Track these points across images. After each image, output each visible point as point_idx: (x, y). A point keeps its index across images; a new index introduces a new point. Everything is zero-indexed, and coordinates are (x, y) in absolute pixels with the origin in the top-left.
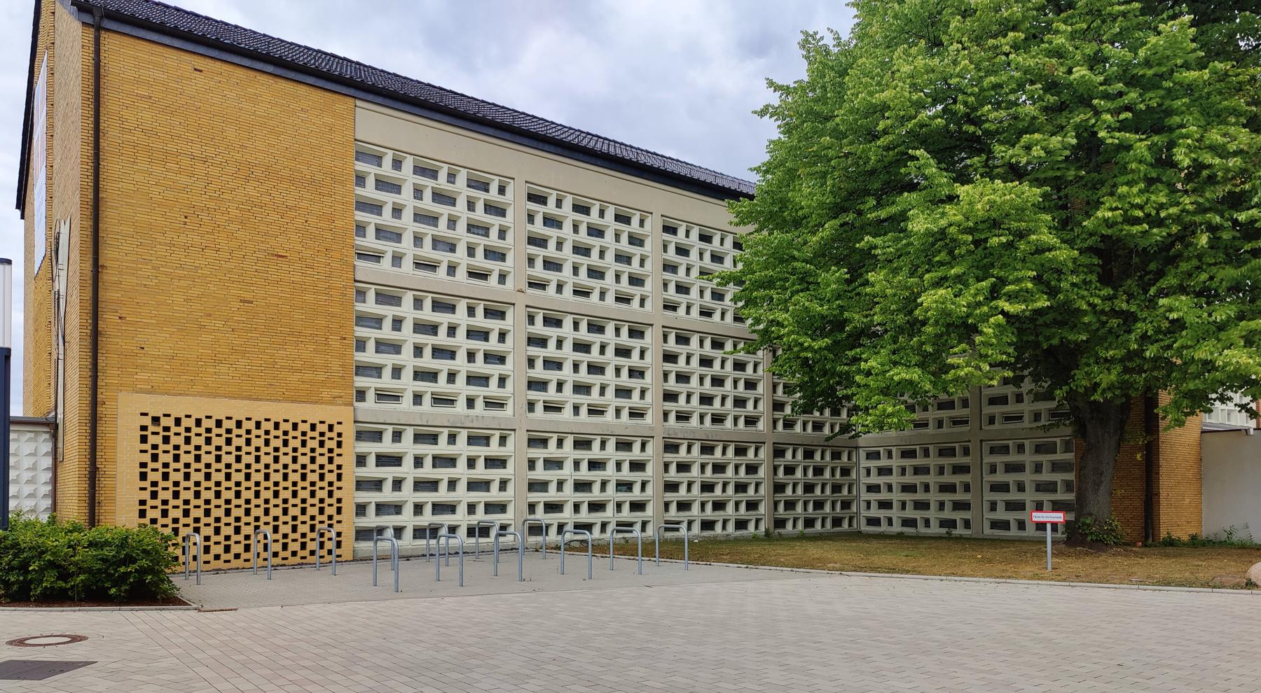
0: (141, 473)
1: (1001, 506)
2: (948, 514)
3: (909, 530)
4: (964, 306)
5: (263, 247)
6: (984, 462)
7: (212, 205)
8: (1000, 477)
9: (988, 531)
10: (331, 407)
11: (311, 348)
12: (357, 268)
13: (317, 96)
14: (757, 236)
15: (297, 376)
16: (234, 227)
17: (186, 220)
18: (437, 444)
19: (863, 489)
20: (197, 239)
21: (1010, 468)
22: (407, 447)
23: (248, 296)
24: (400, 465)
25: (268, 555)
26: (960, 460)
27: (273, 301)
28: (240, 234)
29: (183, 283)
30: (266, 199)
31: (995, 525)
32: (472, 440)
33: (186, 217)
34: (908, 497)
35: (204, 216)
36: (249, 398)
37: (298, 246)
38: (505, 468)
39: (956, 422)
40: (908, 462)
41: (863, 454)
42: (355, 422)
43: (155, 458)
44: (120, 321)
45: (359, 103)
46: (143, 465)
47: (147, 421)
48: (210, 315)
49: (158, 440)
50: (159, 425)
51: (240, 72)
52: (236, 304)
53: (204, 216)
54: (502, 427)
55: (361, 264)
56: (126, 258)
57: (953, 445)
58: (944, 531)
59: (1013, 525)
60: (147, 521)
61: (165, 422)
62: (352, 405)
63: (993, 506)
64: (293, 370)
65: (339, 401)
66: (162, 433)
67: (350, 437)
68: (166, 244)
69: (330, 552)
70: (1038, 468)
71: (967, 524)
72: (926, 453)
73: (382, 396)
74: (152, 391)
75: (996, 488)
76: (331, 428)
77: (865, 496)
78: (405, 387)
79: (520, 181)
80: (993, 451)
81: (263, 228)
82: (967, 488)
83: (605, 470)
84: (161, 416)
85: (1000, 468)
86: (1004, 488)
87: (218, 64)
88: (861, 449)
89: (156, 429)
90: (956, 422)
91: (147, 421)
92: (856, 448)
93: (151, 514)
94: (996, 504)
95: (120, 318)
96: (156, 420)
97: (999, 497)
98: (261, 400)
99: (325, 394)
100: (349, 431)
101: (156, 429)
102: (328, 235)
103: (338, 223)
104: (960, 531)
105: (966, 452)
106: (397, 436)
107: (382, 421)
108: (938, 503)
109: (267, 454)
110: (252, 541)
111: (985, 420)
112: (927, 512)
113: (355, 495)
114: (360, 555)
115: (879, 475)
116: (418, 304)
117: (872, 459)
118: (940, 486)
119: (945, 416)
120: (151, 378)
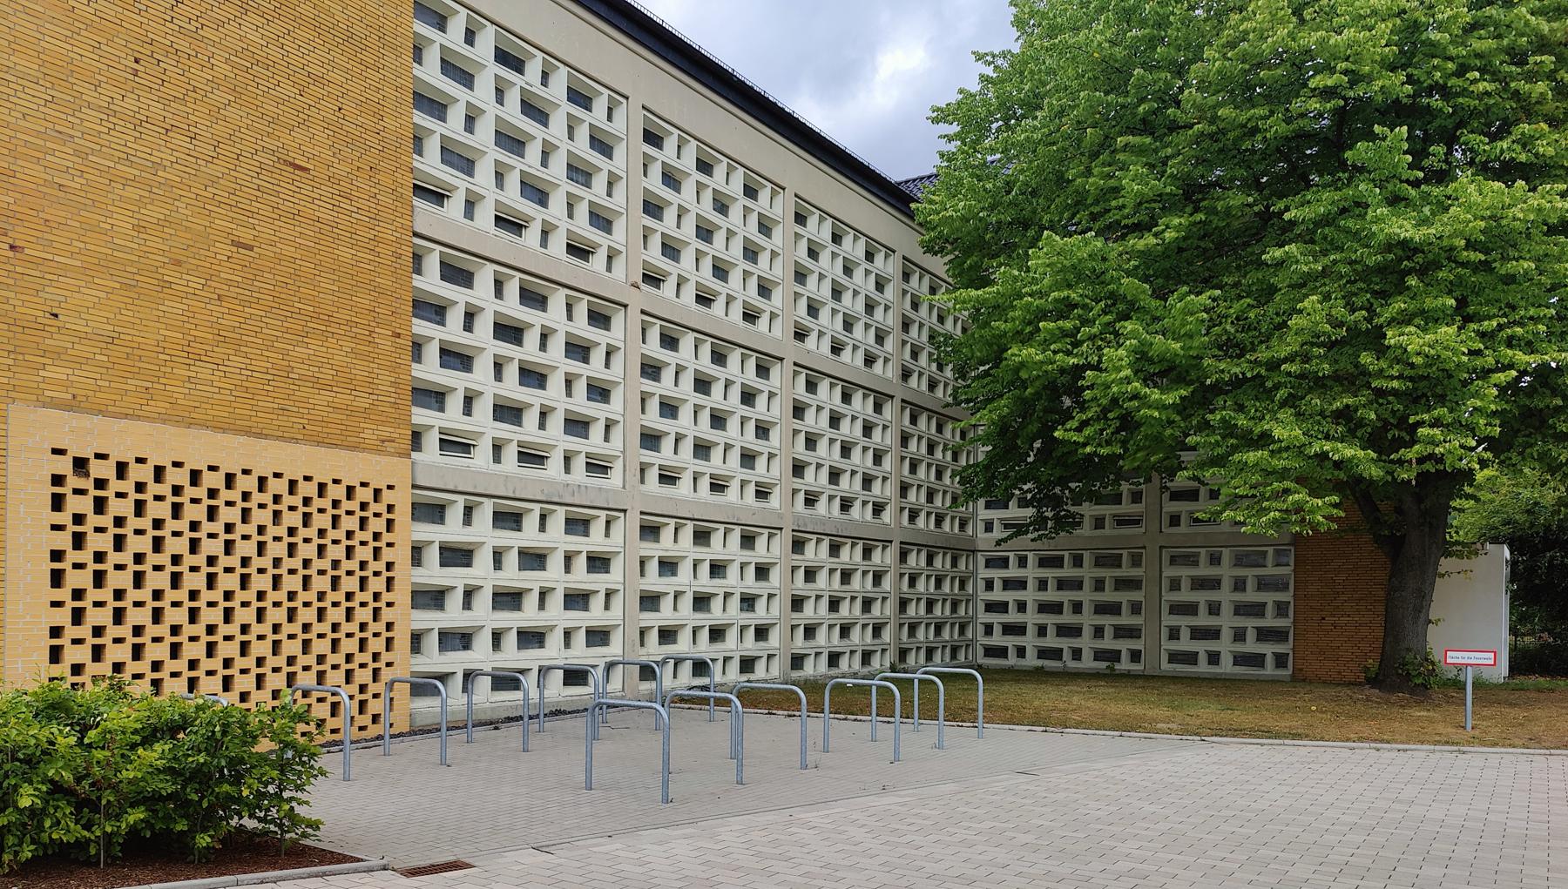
0: (53, 571)
1: (1185, 634)
2: (1108, 643)
3: (1050, 664)
4: (1464, 354)
5: (270, 143)
6: (1164, 575)
7: (183, 44)
8: (1185, 595)
9: (1166, 666)
10: (378, 458)
11: (348, 345)
12: (417, 210)
14: (1281, 205)
15: (326, 397)
16: (220, 96)
17: (136, 66)
18: (519, 530)
19: (981, 607)
20: (157, 108)
21: (1200, 584)
23: (246, 236)
24: (469, 565)
26: (1126, 571)
27: (289, 250)
28: (231, 113)
29: (132, 193)
30: (274, 53)
31: (1174, 657)
33: (137, 61)
34: (1050, 620)
35: (168, 63)
36: (248, 432)
37: (327, 154)
38: (607, 572)
39: (1121, 521)
40: (1050, 574)
41: (981, 561)
42: (414, 486)
43: (79, 541)
44: (11, 254)
46: (57, 555)
47: (64, 466)
48: (178, 263)
49: (85, 505)
50: (87, 475)
52: (225, 249)
53: (168, 63)
54: (610, 506)
55: (419, 203)
56: (21, 123)
58: (1103, 665)
59: (1203, 658)
60: (63, 669)
61: (98, 469)
62: (409, 456)
63: (989, 630)
66: (93, 492)
67: (403, 515)
68: (99, 109)
70: (1239, 585)
71: (1135, 656)
72: (1078, 561)
74: (72, 405)
75: (1177, 609)
77: (985, 617)
78: (481, 430)
79: (636, 102)
80: (1174, 560)
81: (270, 108)
82: (1136, 608)
83: (724, 577)
84: (92, 457)
85: (998, 585)
86: (1190, 609)
88: (979, 554)
89: (81, 483)
90: (1121, 521)
91: (64, 466)
92: (973, 551)
93: (72, 655)
94: (992, 627)
95: (12, 247)
96: (80, 465)
97: (1184, 622)
98: (266, 437)
99: (369, 435)
100: (402, 499)
101: (81, 483)
102: (373, 141)
103: (389, 122)
104: (1125, 665)
105: (1136, 561)
107: (451, 487)
108: (1093, 628)
109: (138, 532)
111: (1166, 520)
112: (1079, 640)
113: (413, 617)
114: (420, 722)
117: (994, 567)
118: (986, 605)
119: (1108, 513)
120: (71, 378)
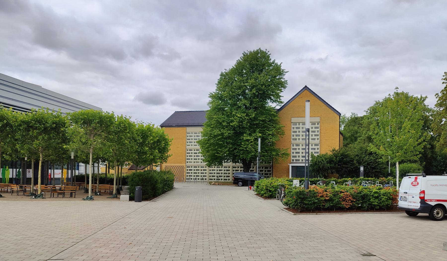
64: (179, 160)
76: (183, 166)
96: (181, 166)
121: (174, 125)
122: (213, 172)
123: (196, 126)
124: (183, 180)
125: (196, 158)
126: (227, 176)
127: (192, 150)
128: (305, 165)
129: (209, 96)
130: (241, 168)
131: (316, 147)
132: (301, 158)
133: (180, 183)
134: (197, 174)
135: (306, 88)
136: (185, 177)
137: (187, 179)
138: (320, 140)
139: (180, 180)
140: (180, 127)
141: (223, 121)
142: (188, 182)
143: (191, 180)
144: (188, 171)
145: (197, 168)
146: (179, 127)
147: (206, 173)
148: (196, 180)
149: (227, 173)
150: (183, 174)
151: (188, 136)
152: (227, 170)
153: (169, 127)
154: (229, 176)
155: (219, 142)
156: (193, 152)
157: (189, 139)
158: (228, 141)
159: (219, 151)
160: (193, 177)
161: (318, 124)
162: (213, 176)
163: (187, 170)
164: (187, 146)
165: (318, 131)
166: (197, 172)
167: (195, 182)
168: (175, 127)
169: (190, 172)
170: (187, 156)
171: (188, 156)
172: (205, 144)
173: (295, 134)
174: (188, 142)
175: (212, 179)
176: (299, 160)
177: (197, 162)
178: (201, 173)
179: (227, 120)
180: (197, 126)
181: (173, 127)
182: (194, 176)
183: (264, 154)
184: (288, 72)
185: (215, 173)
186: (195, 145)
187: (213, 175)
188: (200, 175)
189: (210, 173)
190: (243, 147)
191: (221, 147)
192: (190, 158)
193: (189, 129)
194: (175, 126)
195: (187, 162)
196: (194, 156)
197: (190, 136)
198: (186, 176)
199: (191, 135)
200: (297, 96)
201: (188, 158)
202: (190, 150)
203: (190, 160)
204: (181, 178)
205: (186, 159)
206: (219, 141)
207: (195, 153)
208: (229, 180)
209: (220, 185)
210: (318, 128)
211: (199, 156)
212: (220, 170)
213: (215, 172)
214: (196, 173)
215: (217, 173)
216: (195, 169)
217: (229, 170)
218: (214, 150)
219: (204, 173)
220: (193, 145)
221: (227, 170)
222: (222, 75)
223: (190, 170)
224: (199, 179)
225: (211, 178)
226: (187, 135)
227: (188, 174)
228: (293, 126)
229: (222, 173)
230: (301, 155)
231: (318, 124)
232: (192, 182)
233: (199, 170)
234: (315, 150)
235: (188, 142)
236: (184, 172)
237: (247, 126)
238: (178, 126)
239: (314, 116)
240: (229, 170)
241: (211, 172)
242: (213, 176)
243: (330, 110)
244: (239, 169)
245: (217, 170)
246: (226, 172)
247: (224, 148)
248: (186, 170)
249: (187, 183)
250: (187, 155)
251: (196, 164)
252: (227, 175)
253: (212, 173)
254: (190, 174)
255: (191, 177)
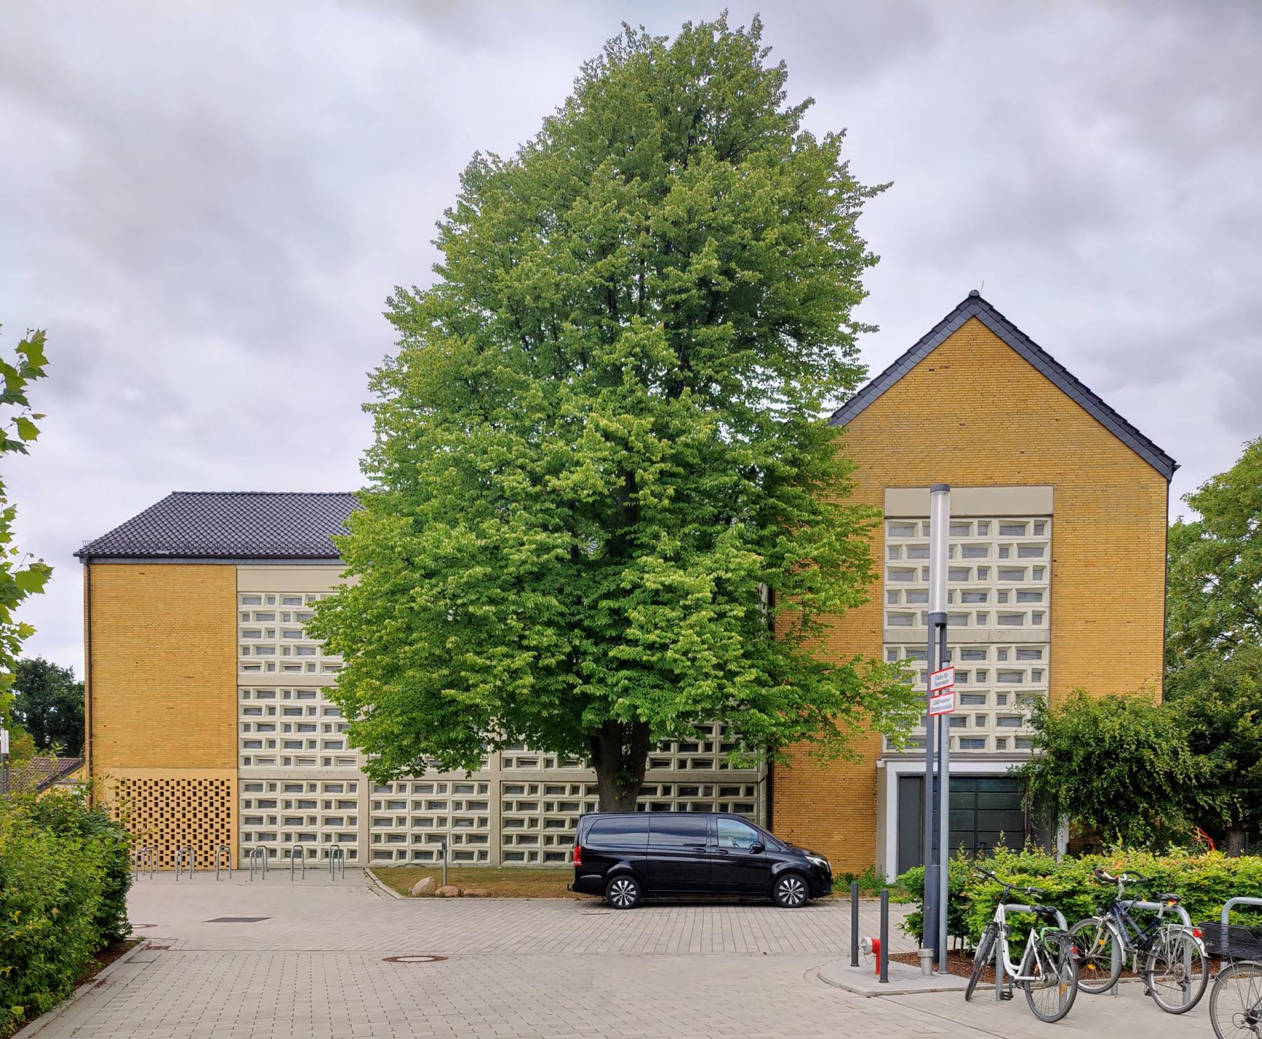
7: (151, 653)
13: (211, 570)
22: (279, 795)
23: (171, 705)
25: (197, 863)
29: (136, 702)
32: (724, 792)
45: (239, 567)
51: (165, 568)
57: (737, 785)
64: (197, 747)
65: (227, 766)
69: (167, 863)
73: (262, 760)
76: (223, 783)
87: (153, 567)
96: (211, 783)
106: (667, 791)
110: (176, 855)
115: (300, 807)
116: (1002, 654)
121: (160, 552)
122: (394, 813)
123: (295, 561)
124: (224, 859)
125: (293, 735)
126: (473, 838)
127: (271, 694)
128: (930, 767)
129: (390, 310)
130: (589, 791)
131: (1028, 665)
132: (992, 731)
133: (201, 875)
134: (305, 828)
135: (974, 309)
136: (233, 841)
137: (247, 852)
138: (1051, 623)
139: (206, 859)
140: (199, 561)
141: (503, 465)
142: (254, 869)
143: (271, 860)
144: (254, 811)
145: (305, 795)
146: (193, 561)
147: (353, 820)
148: (297, 860)
149: (470, 822)
150: (223, 826)
151: (246, 616)
152: (472, 805)
153: (136, 561)
154: (482, 838)
155: (472, 602)
156: (278, 702)
157: (255, 633)
158: (531, 599)
159: (473, 669)
160: (278, 844)
161: (1039, 528)
162: (393, 838)
163: (248, 804)
164: (243, 673)
165: (1038, 571)
166: (304, 813)
167: (293, 869)
168: (167, 561)
169: (265, 812)
170: (241, 727)
171: (247, 727)
172: (369, 622)
173: (903, 586)
174: (246, 650)
175: (388, 855)
176: (979, 742)
177: (302, 760)
178: (328, 821)
179: (524, 456)
180: (301, 561)
181: (160, 561)
182: (288, 837)
183: (764, 691)
184: (882, 188)
185: (402, 821)
186: (287, 668)
187: (394, 829)
188: (320, 829)
189: (378, 821)
190: (634, 643)
191: (480, 644)
192: (263, 736)
193: (252, 577)
194: (171, 556)
195: (247, 761)
196: (287, 727)
197: (260, 616)
198: (242, 837)
199: (264, 607)
200: (921, 353)
201: (253, 735)
202: (260, 694)
203: (264, 751)
204: (212, 848)
205: (241, 744)
206: (473, 597)
207: (288, 711)
208: (483, 855)
209: (472, 896)
210: (1035, 550)
211: (315, 726)
212: (432, 805)
213: (407, 812)
214: (299, 821)
215: (418, 821)
216: (293, 796)
217: (482, 805)
218: (440, 662)
219: (342, 819)
220: (277, 667)
221: (472, 805)
222: (474, 179)
223: (262, 803)
224: (313, 853)
225: (383, 846)
226: (243, 608)
227: (254, 828)
228: (890, 540)
229: (442, 821)
230: (991, 708)
231: (1039, 528)
232: (278, 872)
233: (313, 804)
234: (1020, 681)
235: (246, 650)
236: (228, 815)
237: (661, 500)
238: (185, 556)
239: (1018, 478)
240: (482, 805)
241: (383, 813)
242: (393, 838)
243: (1114, 443)
244: (581, 797)
245: (417, 805)
246: (463, 813)
247: (502, 649)
248: (242, 804)
249: (247, 874)
250: (245, 719)
251: (295, 771)
252: (475, 829)
253: (388, 821)
254: (265, 828)
255: (270, 844)
